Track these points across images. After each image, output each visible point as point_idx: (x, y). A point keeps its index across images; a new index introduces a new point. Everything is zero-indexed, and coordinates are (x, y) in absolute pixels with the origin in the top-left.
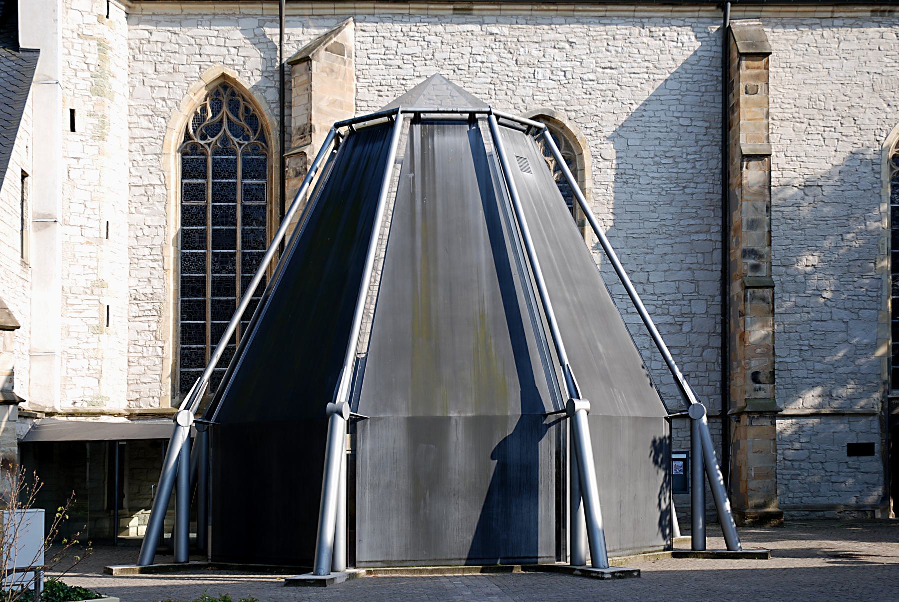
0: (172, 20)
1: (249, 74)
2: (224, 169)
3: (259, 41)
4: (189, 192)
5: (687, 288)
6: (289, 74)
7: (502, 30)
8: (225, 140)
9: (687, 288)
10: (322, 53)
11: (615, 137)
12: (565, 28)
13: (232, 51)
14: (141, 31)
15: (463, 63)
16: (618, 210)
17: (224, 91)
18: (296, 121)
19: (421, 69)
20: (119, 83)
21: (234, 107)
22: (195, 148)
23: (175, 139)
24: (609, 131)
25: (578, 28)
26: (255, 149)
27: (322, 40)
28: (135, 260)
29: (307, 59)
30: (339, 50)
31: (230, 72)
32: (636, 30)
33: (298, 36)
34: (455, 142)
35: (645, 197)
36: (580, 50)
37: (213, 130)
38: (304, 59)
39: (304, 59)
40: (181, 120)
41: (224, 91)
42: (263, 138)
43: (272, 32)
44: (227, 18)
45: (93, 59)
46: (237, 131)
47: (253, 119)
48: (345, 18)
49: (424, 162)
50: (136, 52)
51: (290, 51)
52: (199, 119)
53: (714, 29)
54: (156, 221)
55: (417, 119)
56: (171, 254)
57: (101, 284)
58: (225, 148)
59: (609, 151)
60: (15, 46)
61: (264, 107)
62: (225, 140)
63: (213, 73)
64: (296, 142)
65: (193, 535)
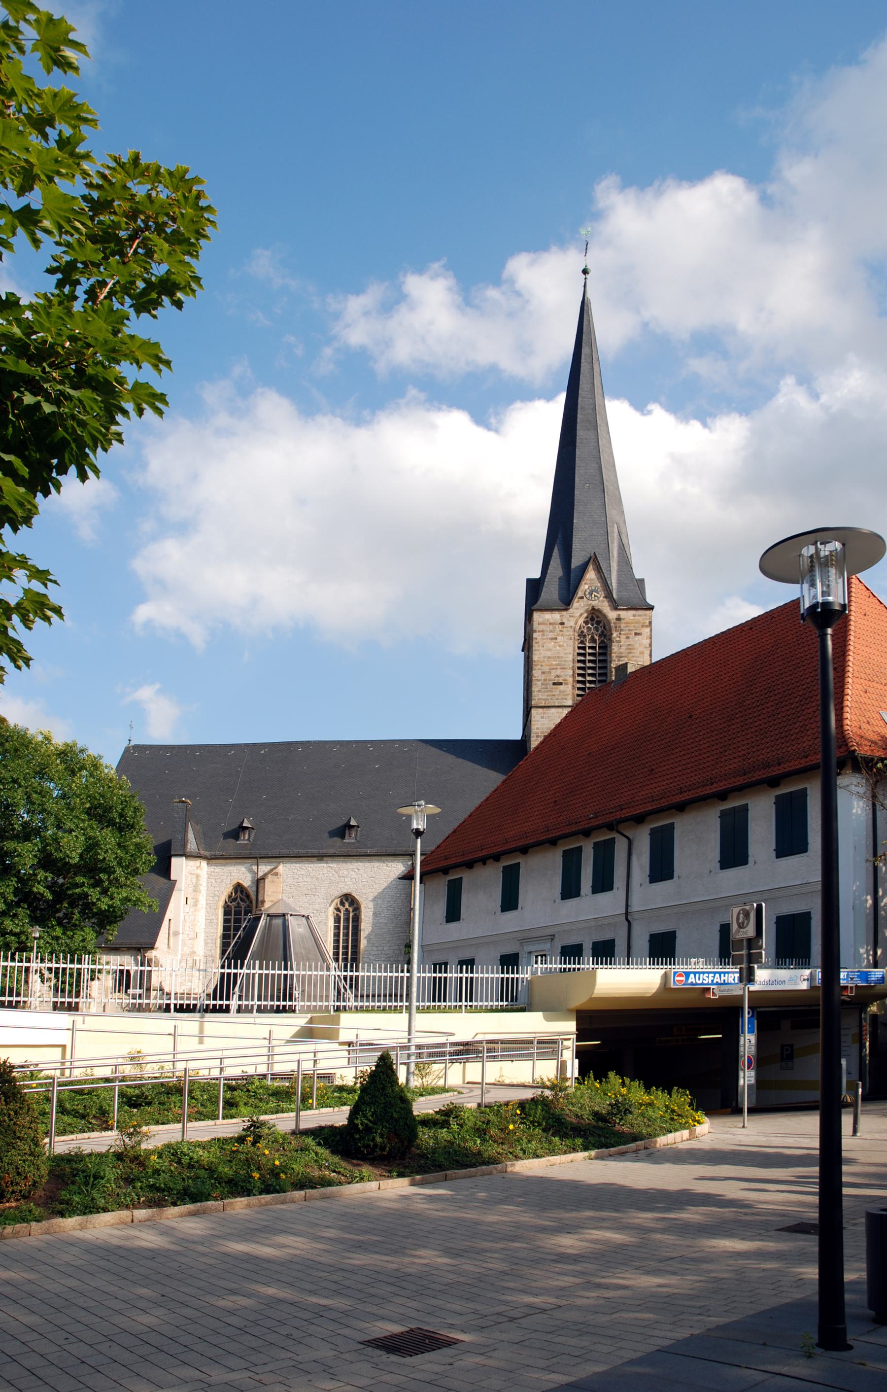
0: (222, 865)
1: (247, 882)
2: (238, 913)
3: (250, 871)
4: (226, 921)
5: (397, 952)
6: (259, 882)
7: (334, 865)
8: (238, 903)
9: (397, 952)
10: (270, 876)
11: (373, 900)
12: (356, 864)
13: (240, 874)
14: (212, 869)
15: (320, 877)
16: (374, 925)
17: (239, 888)
18: (260, 899)
19: (305, 879)
20: (203, 888)
21: (242, 892)
22: (228, 906)
23: (221, 903)
24: (371, 898)
25: (361, 864)
26: (248, 906)
27: (272, 870)
28: (206, 944)
29: (264, 879)
30: (276, 874)
31: (241, 882)
32: (381, 864)
33: (264, 869)
34: (278, 922)
35: (383, 921)
36: (361, 872)
37: (234, 900)
38: (263, 878)
39: (263, 878)
40: (224, 897)
41: (239, 888)
42: (251, 902)
43: (255, 868)
44: (240, 864)
45: (194, 881)
46: (242, 900)
47: (248, 896)
48: (279, 863)
49: (268, 928)
50: (210, 875)
51: (261, 874)
52: (230, 896)
53: (410, 863)
54: (214, 931)
55: (268, 915)
56: (219, 942)
57: (194, 952)
58: (238, 906)
59: (371, 905)
60: (170, 879)
61: (251, 893)
62: (238, 903)
63: (235, 882)
64: (260, 905)
65: (310, 1101)
